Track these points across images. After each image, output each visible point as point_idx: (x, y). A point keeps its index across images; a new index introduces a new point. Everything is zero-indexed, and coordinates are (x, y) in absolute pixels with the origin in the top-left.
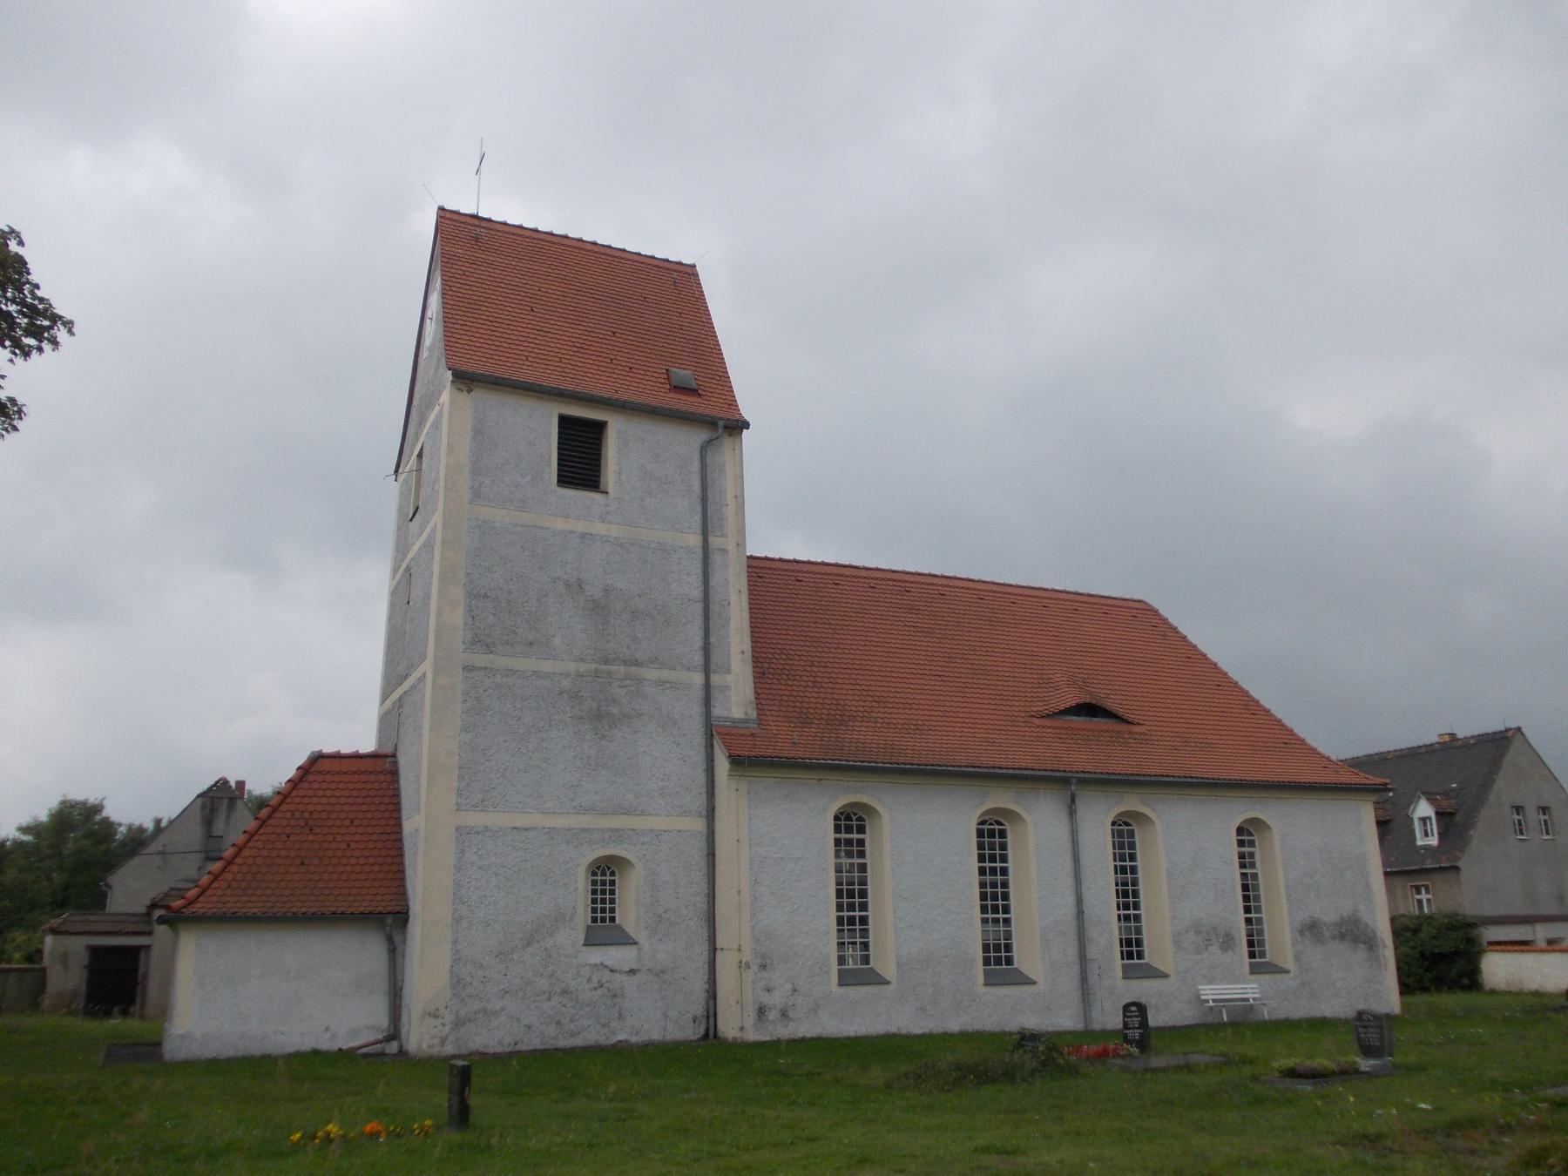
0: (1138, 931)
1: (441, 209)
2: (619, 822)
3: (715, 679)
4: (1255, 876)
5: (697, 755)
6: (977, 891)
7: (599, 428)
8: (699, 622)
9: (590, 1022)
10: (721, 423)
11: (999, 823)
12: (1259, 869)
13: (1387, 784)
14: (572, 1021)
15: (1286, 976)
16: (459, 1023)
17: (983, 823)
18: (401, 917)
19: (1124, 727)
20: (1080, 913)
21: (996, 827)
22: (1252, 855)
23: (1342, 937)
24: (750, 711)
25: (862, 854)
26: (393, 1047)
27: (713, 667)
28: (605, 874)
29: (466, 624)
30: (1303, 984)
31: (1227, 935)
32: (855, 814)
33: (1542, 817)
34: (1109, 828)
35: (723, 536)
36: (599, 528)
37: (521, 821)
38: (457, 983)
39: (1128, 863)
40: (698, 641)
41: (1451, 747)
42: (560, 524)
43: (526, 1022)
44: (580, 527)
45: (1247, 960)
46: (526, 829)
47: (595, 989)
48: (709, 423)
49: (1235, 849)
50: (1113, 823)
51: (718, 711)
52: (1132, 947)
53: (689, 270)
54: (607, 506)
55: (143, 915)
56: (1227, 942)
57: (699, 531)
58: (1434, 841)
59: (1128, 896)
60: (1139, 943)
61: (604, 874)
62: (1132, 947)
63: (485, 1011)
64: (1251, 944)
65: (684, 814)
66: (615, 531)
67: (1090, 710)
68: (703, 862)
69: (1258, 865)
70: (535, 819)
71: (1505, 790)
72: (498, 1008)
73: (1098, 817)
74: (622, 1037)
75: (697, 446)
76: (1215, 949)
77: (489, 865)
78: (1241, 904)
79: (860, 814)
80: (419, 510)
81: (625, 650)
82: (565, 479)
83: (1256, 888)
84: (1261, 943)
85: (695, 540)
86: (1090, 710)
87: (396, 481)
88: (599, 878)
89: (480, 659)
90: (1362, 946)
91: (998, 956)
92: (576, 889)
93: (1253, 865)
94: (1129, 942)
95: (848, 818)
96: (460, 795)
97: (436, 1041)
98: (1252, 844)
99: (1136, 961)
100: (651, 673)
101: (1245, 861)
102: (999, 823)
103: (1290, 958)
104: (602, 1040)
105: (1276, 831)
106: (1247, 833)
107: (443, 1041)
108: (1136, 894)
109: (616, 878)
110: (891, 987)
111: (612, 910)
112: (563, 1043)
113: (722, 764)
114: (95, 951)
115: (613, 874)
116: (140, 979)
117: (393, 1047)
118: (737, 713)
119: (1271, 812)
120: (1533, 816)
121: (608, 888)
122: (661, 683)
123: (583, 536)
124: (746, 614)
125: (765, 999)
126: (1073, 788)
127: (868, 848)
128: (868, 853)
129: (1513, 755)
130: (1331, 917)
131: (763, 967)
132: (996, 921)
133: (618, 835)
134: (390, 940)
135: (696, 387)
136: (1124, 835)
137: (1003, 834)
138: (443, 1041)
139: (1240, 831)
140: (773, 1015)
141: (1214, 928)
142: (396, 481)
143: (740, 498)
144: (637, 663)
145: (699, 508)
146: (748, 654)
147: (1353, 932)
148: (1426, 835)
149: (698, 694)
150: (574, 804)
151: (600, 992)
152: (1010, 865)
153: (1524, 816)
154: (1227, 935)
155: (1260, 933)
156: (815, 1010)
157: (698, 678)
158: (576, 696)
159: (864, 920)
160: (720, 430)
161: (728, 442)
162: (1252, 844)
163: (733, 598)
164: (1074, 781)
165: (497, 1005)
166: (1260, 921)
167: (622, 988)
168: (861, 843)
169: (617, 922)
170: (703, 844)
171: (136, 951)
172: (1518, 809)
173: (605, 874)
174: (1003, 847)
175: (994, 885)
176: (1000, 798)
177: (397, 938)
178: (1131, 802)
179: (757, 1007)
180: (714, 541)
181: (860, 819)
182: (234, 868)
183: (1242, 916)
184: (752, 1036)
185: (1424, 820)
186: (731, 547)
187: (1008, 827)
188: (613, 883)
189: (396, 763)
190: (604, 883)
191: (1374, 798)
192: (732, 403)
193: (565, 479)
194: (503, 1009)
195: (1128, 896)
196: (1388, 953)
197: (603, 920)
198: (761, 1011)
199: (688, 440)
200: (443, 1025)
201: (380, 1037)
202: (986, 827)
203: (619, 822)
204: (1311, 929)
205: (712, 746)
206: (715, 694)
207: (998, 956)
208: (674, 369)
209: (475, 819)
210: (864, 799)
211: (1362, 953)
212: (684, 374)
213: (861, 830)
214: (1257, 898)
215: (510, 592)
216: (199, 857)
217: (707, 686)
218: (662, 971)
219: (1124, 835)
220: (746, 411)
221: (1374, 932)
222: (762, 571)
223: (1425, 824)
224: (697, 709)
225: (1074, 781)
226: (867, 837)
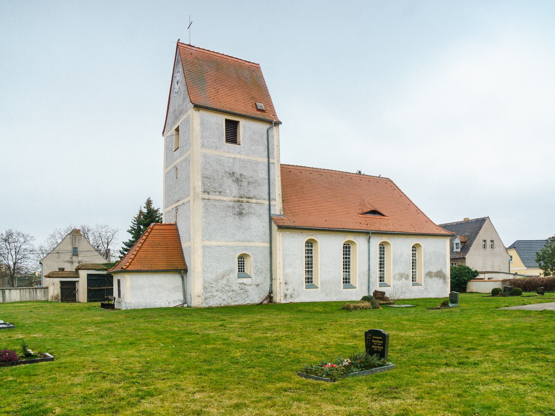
0: (349, 275)
1: (179, 45)
2: (247, 244)
3: (272, 203)
4: (415, 260)
5: (267, 225)
6: (342, 263)
7: (237, 123)
8: (267, 186)
9: (239, 299)
10: (274, 122)
11: (349, 245)
12: (417, 258)
13: (454, 234)
14: (235, 298)
15: (421, 286)
16: (206, 299)
17: (344, 245)
18: (186, 271)
19: (382, 217)
20: (369, 269)
21: (348, 246)
22: (415, 254)
23: (437, 276)
24: (281, 212)
25: (311, 253)
26: (186, 305)
27: (271, 199)
28: (242, 259)
29: (202, 186)
30: (425, 289)
31: (407, 275)
32: (310, 242)
33: (491, 243)
34: (378, 246)
35: (274, 159)
36: (239, 156)
37: (219, 243)
38: (205, 288)
39: (382, 256)
40: (267, 192)
41: (467, 222)
42: (227, 155)
43: (223, 298)
44: (233, 156)
45: (412, 282)
46: (221, 246)
47: (241, 290)
48: (270, 122)
49: (411, 252)
50: (379, 245)
51: (272, 212)
52: (382, 279)
53: (257, 66)
54: (241, 149)
55: (75, 272)
56: (407, 278)
57: (267, 157)
58: (459, 250)
59: (382, 265)
60: (349, 279)
61: (241, 259)
62: (382, 279)
63: (212, 295)
64: (413, 278)
65: (264, 242)
66: (242, 157)
67: (374, 212)
68: (269, 255)
69: (417, 256)
70: (223, 243)
71: (482, 235)
72: (216, 295)
73: (376, 242)
74: (248, 302)
75: (266, 130)
76: (403, 279)
77: (212, 256)
78: (411, 267)
79: (312, 242)
80: (179, 148)
81: (246, 194)
82: (228, 141)
83: (415, 263)
84: (415, 278)
85: (266, 160)
86: (374, 212)
87: (163, 136)
88: (240, 260)
89: (206, 196)
90: (442, 278)
91: (346, 281)
92: (235, 263)
93: (415, 257)
94: (346, 279)
95: (308, 243)
96: (203, 237)
97: (200, 303)
98: (415, 251)
99: (382, 282)
100: (254, 201)
101: (414, 255)
102: (349, 245)
103: (423, 282)
104: (243, 303)
105: (423, 247)
106: (310, 244)
107: (202, 304)
108: (349, 265)
109: (245, 260)
110: (319, 289)
111: (244, 269)
112: (232, 304)
113: (275, 227)
114: (62, 283)
115: (244, 259)
116: (77, 291)
117: (186, 305)
118: (278, 213)
119: (422, 242)
120: (489, 243)
121: (242, 262)
122: (257, 203)
123: (234, 158)
124: (280, 183)
125: (287, 292)
126: (370, 235)
127: (313, 252)
128: (313, 253)
129: (485, 225)
130: (435, 271)
131: (286, 283)
132: (346, 272)
133: (246, 248)
134: (182, 277)
135: (265, 109)
136: (310, 244)
137: (349, 248)
138: (202, 304)
139: (413, 247)
140: (288, 296)
141: (404, 273)
142: (163, 136)
143: (278, 146)
144: (249, 198)
145: (267, 150)
146: (281, 196)
147: (440, 275)
148: (457, 248)
149: (267, 207)
150: (234, 239)
151: (242, 290)
152: (351, 256)
153: (486, 243)
154: (407, 275)
155: (415, 275)
156: (299, 295)
157: (267, 203)
158: (233, 207)
159: (311, 271)
160: (273, 124)
161: (275, 128)
162: (415, 251)
163: (277, 179)
164: (371, 233)
165: (215, 294)
166: (415, 272)
167: (248, 290)
168: (311, 250)
169: (245, 272)
170: (269, 250)
171: (74, 283)
172: (485, 241)
173: (242, 259)
174: (349, 251)
175: (346, 262)
176: (350, 238)
177: (184, 277)
178: (385, 239)
179: (284, 294)
180: (271, 161)
181: (312, 243)
182: (137, 257)
183: (411, 270)
184: (283, 301)
185: (457, 244)
186: (276, 162)
187: (351, 246)
188: (244, 261)
189: (177, 227)
190: (241, 261)
191: (450, 238)
192: (275, 115)
193: (228, 141)
194: (217, 295)
195: (382, 265)
196: (449, 281)
197: (241, 271)
198: (286, 295)
199: (264, 127)
200: (202, 299)
201: (181, 304)
202: (345, 246)
203: (247, 244)
204: (429, 274)
205: (271, 222)
206: (272, 207)
207: (346, 281)
208: (258, 103)
209: (207, 243)
210: (313, 238)
211: (442, 281)
212: (261, 105)
213: (312, 246)
214: (415, 266)
215: (214, 176)
216: (71, 254)
217: (270, 205)
218: (258, 285)
219: (382, 247)
220: (280, 118)
221: (445, 275)
222: (286, 170)
223: (457, 245)
224: (267, 212)
225: (371, 233)
226: (313, 248)
